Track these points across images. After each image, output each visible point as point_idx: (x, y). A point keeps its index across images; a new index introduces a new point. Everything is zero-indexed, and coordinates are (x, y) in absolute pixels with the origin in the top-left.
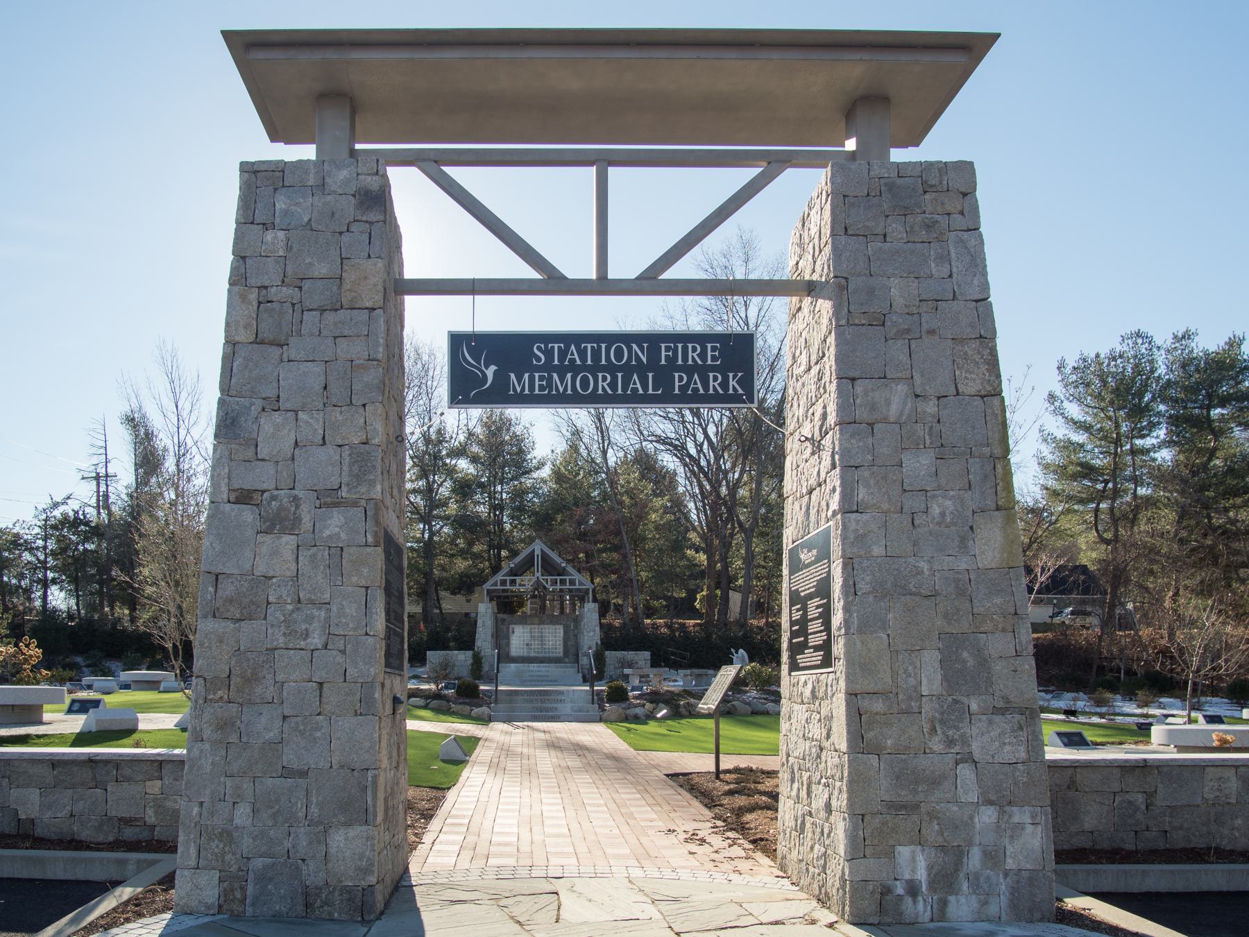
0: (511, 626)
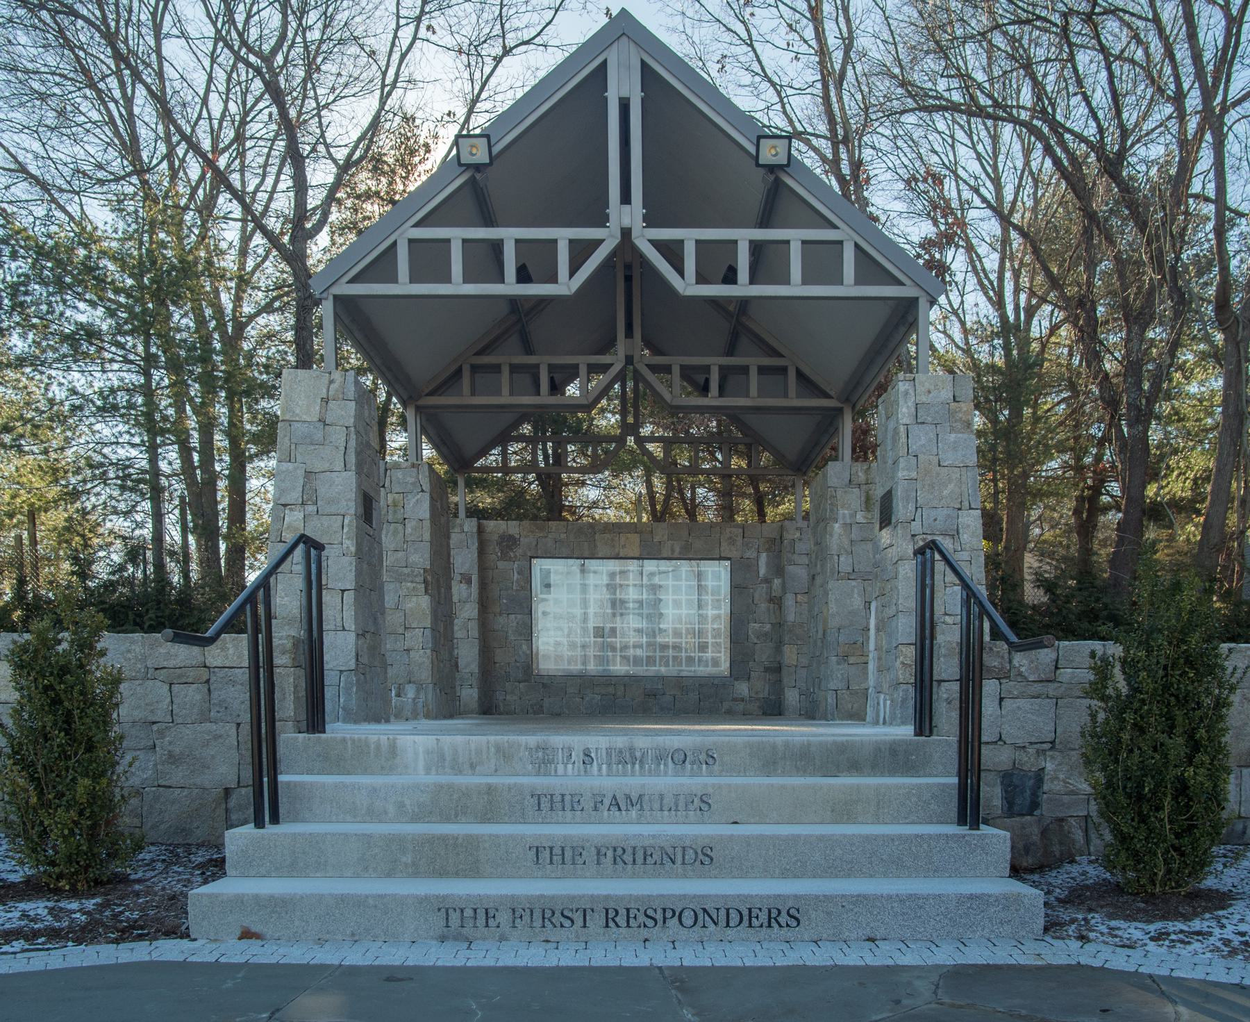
0: (539, 565)
